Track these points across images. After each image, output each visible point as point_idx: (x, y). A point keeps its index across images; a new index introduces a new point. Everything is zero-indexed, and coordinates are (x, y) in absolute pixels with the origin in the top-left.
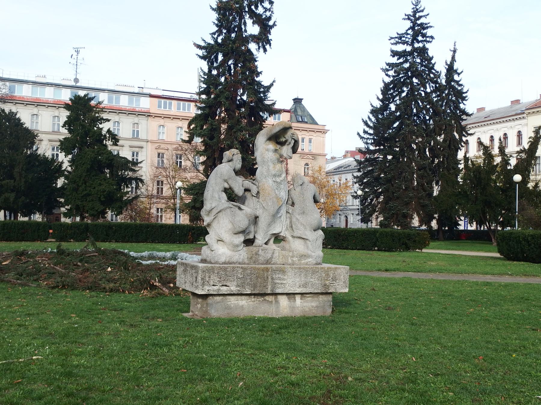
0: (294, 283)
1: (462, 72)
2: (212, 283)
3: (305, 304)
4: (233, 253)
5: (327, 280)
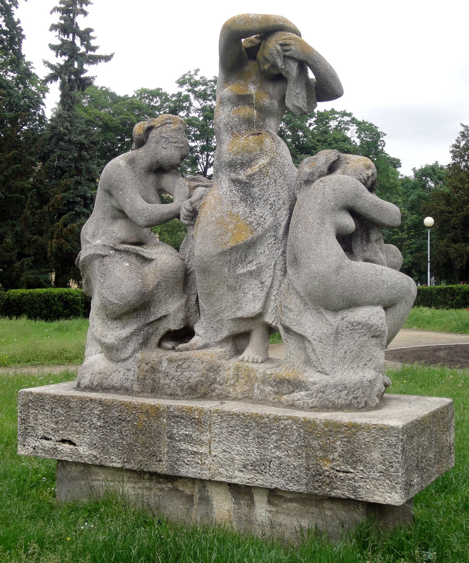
0: (228, 456)
1: (107, 58)
2: (40, 433)
3: (281, 519)
4: (113, 366)
5: (325, 458)
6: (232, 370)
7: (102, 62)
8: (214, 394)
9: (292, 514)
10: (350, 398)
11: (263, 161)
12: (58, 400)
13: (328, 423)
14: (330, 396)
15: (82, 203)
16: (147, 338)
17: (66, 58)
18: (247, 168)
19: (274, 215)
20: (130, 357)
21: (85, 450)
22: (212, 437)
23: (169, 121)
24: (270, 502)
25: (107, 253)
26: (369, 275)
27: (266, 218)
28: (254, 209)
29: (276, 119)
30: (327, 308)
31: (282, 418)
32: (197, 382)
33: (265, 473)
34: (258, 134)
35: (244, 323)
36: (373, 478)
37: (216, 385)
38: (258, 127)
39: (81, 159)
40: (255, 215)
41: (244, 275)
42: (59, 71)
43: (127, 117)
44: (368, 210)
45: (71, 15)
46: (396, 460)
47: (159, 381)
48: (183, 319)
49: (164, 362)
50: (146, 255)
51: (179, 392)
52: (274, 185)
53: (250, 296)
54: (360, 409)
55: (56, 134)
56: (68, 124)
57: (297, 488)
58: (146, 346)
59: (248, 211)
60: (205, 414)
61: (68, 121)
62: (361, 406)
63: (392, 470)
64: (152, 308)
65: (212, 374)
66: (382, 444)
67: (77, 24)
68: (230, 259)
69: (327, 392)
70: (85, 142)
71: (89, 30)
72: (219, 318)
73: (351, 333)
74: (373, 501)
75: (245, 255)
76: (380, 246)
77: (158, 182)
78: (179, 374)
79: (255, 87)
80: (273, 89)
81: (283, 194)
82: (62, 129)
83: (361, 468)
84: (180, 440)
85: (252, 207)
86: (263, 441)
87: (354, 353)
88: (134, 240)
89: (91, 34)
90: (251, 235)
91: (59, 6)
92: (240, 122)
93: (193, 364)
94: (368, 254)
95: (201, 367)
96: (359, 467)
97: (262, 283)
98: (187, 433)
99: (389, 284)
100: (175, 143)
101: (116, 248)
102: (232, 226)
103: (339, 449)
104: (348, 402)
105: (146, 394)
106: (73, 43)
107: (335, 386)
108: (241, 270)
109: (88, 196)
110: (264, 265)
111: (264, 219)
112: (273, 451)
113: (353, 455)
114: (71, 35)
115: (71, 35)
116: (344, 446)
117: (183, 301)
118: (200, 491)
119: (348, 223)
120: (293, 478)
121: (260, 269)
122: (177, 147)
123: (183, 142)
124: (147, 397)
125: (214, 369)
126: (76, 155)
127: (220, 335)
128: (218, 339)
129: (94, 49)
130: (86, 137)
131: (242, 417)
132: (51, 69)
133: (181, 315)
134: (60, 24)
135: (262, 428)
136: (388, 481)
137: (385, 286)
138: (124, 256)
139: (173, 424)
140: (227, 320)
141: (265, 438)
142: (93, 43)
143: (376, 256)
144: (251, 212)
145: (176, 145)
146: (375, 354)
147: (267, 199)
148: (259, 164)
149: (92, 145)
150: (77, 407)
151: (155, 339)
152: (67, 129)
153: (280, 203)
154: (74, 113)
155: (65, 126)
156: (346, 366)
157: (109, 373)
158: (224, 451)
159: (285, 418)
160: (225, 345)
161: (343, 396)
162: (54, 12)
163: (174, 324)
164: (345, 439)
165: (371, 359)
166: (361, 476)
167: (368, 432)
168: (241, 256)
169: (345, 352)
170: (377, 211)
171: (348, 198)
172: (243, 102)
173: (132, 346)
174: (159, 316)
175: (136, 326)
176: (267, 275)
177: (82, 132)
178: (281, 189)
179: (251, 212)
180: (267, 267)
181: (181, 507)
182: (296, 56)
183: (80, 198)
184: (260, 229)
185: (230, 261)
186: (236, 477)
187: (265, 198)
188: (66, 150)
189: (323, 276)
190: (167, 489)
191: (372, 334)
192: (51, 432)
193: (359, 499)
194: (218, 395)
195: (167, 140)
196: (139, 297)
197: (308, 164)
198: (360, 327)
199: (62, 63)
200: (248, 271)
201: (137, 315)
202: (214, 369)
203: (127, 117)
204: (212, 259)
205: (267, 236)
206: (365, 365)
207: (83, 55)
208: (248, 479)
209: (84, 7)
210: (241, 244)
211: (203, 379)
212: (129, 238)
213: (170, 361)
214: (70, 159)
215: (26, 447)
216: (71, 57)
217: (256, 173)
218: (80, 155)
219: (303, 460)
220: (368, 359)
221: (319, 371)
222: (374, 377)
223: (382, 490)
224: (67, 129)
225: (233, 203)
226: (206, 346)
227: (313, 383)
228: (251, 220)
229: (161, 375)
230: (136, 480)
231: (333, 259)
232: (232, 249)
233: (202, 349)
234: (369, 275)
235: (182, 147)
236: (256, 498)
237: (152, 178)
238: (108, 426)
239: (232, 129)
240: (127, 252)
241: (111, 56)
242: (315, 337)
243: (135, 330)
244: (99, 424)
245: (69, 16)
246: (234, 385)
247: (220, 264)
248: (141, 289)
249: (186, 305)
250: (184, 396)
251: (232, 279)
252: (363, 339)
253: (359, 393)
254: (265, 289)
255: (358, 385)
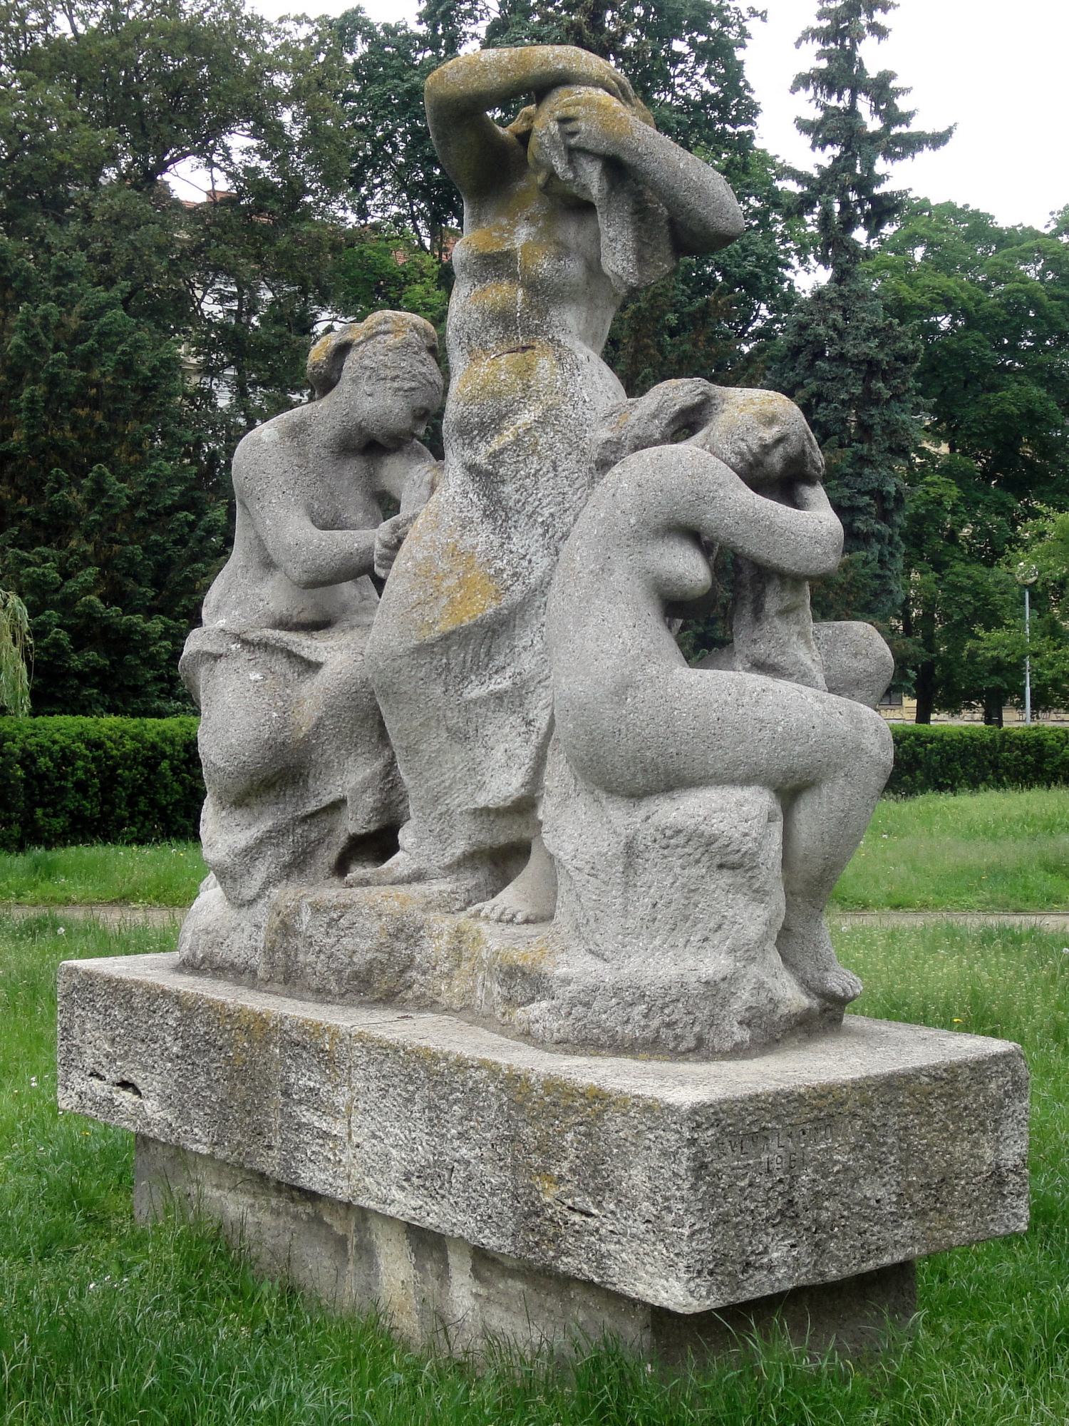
1: (938, 140)
6: (446, 938)
7: (926, 149)
8: (410, 995)
9: (514, 1308)
10: (655, 1023)
11: (527, 417)
12: (120, 990)
13: (553, 1086)
14: (604, 1016)
15: (873, 510)
16: (304, 852)
17: (835, 151)
18: (492, 436)
19: (552, 551)
20: (259, 896)
21: (155, 1108)
22: (352, 1099)
23: (383, 328)
24: (476, 1274)
25: (222, 650)
26: (715, 706)
27: (534, 558)
28: (509, 538)
29: (583, 308)
30: (611, 791)
31: (470, 1063)
32: (370, 962)
33: (443, 1197)
34: (524, 349)
35: (501, 823)
36: (634, 1236)
37: (414, 974)
38: (527, 331)
39: (870, 399)
40: (511, 552)
41: (482, 702)
42: (818, 186)
43: (1021, 286)
44: (732, 534)
45: (847, 42)
46: (678, 1194)
47: (296, 955)
48: (373, 809)
49: (304, 910)
50: (305, 653)
51: (333, 986)
52: (551, 475)
53: (499, 754)
54: (683, 1053)
55: (808, 342)
56: (836, 316)
57: (498, 1242)
58: (302, 871)
59: (496, 543)
60: (342, 1041)
61: (839, 307)
62: (682, 1048)
63: (670, 1218)
64: (311, 781)
65: (404, 945)
66: (649, 1148)
67: (861, 62)
68: (448, 664)
69: (596, 1006)
70: (881, 356)
71: (886, 77)
72: (442, 808)
73: (665, 857)
74: (634, 1295)
75: (488, 653)
76: (798, 628)
77: (371, 476)
78: (332, 940)
79: (533, 229)
80: (571, 232)
81: (575, 498)
82: (821, 330)
83: (612, 1206)
84: (300, 1102)
85: (505, 532)
86: (437, 1117)
87: (673, 906)
88: (307, 616)
89: (893, 84)
90: (494, 603)
91: (817, 24)
92: (484, 322)
93: (360, 919)
94: (761, 650)
95: (376, 927)
96: (608, 1203)
97: (529, 723)
98: (312, 1084)
99: (780, 729)
100: (394, 379)
101: (244, 636)
102: (452, 581)
103: (572, 1153)
104: (648, 1034)
105: (277, 987)
106: (852, 111)
107: (617, 992)
108: (475, 691)
109: (889, 493)
110: (532, 678)
111: (530, 561)
112: (456, 1143)
113: (596, 1172)
114: (847, 93)
115: (847, 93)
116: (580, 1147)
117: (378, 765)
118: (358, 1230)
119: (680, 570)
120: (490, 1217)
121: (522, 687)
122: (399, 389)
123: (414, 376)
124: (276, 993)
125: (405, 932)
126: (857, 390)
127: (449, 851)
128: (447, 861)
129: (905, 118)
130: (881, 346)
131: (402, 1053)
132: (799, 183)
133: (369, 800)
134: (817, 70)
135: (434, 1086)
136: (660, 1246)
137: (767, 734)
138: (261, 656)
139: (289, 1061)
140: (461, 814)
141: (441, 1111)
142: (902, 104)
143: (783, 653)
144: (502, 545)
145: (396, 385)
146: (730, 913)
147: (533, 512)
148: (519, 423)
149: (900, 364)
150: (142, 1008)
151: (329, 856)
152: (835, 328)
153: (567, 520)
154: (853, 286)
155: (830, 322)
156: (657, 942)
157: (223, 932)
158: (374, 1136)
159: (475, 1063)
160: (468, 874)
161: (637, 1018)
162: (804, 42)
163: (354, 822)
164: (582, 1129)
165: (720, 927)
166: (611, 1228)
167: (624, 1115)
168: (476, 655)
169: (654, 905)
170: (757, 536)
171: (677, 504)
172: (496, 270)
173: (261, 871)
174: (327, 800)
175: (270, 823)
176: (541, 704)
177: (874, 332)
178: (570, 486)
179: (502, 545)
180: (539, 682)
181: (327, 1263)
182: (590, 146)
183: (867, 498)
184: (518, 587)
185: (447, 667)
186: (393, 1201)
187: (529, 508)
188: (833, 379)
189: (583, 708)
190: (304, 1217)
191: (717, 861)
192: (104, 1061)
193: (608, 1286)
194: (418, 998)
195: (375, 375)
196: (269, 754)
197: (610, 419)
198: (681, 840)
199: (827, 163)
200: (491, 694)
201: (277, 797)
202: (405, 932)
203: (1021, 286)
204: (396, 664)
205: (537, 604)
206: (706, 940)
207: (874, 138)
208: (415, 1209)
209: (879, 16)
210: (468, 627)
211: (383, 957)
212: (295, 613)
213: (316, 909)
214: (843, 402)
215: (70, 1092)
216: (848, 146)
217: (505, 449)
218: (868, 390)
219: (507, 1174)
220: (712, 925)
221: (591, 951)
222: (727, 971)
223: (651, 1269)
224: (835, 328)
225: (465, 524)
226: (418, 877)
227: (563, 981)
228: (499, 564)
229: (299, 942)
230: (256, 1189)
231: (610, 663)
232: (446, 637)
233: (409, 882)
234: (715, 706)
235: (412, 389)
236: (453, 1259)
237: (354, 467)
238: (190, 1057)
239: (470, 339)
240: (264, 646)
241: (949, 132)
242: (579, 864)
243: (270, 831)
244: (175, 1049)
245: (843, 46)
246: (448, 975)
247: (421, 675)
248: (273, 735)
249: (388, 774)
250: (343, 995)
251: (456, 714)
252: (695, 871)
253: (678, 1013)
254: (533, 737)
255: (673, 991)
